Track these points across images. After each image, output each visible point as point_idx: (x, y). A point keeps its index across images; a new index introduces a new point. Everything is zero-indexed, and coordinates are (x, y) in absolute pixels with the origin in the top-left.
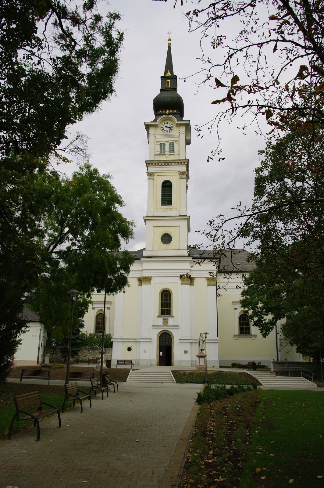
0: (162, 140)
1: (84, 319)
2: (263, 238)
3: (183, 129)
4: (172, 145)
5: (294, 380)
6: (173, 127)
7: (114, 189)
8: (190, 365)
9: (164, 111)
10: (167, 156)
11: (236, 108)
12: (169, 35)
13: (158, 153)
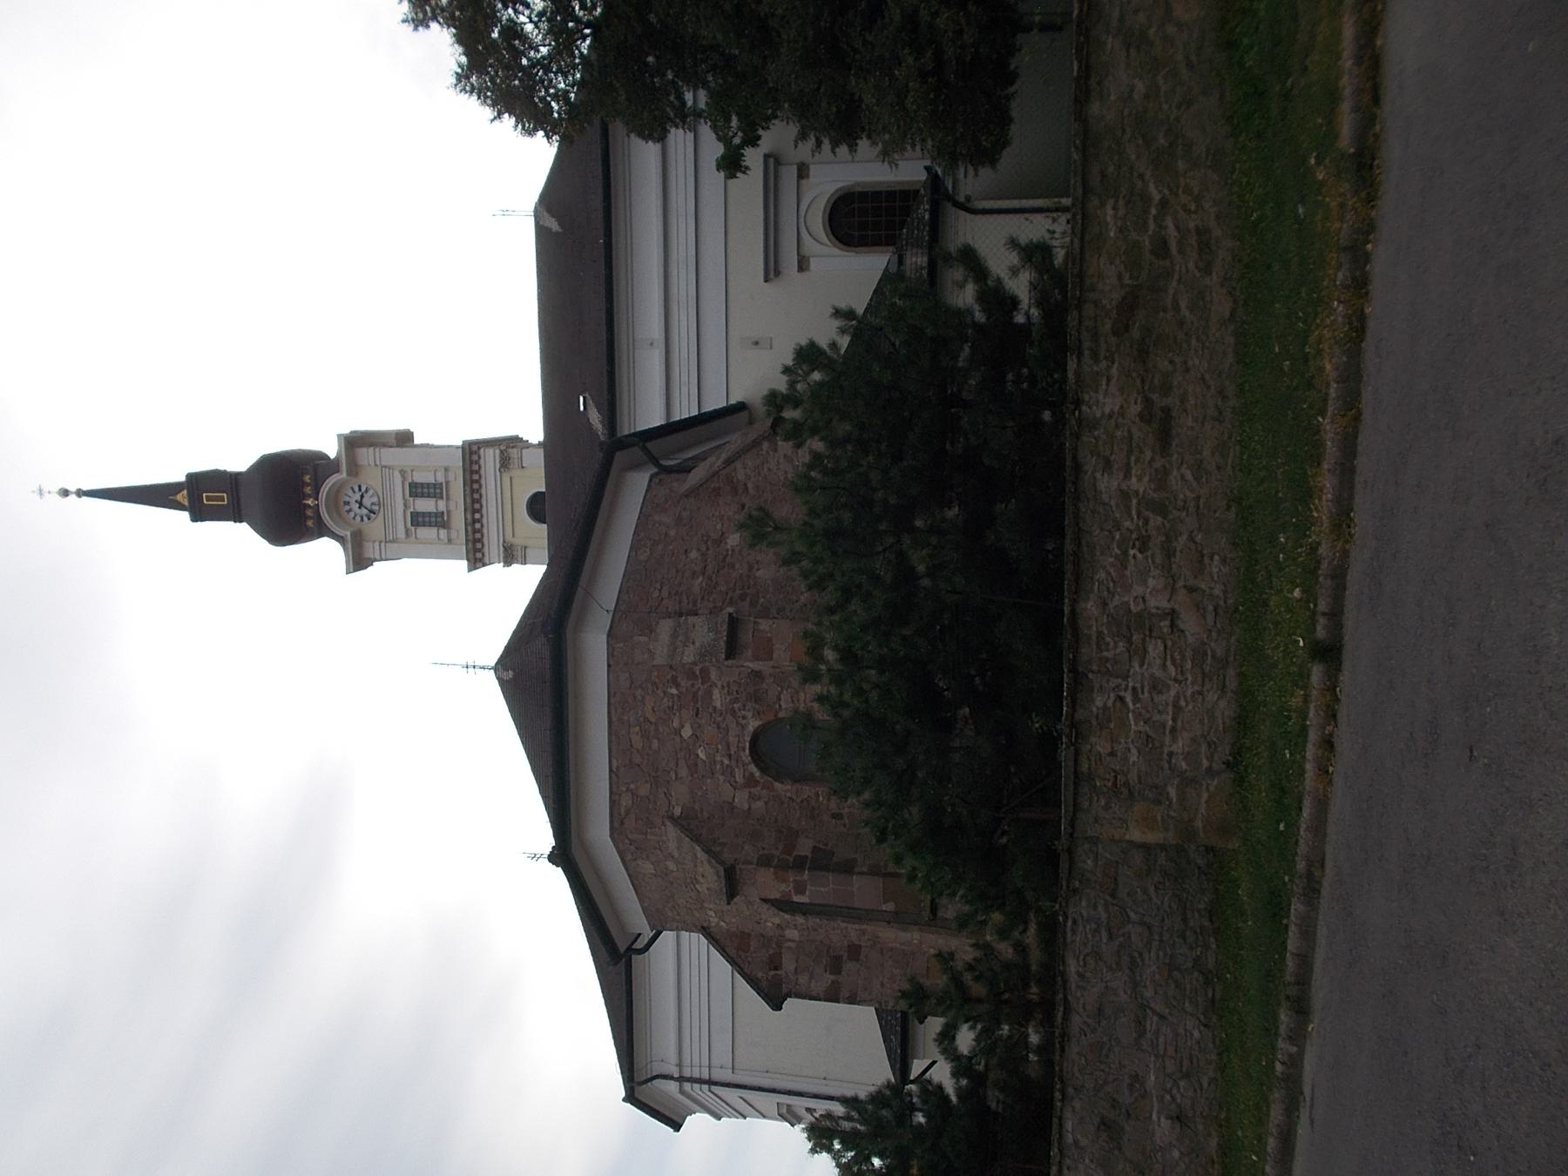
0: (400, 524)
1: (949, 1065)
3: (365, 455)
4: (417, 490)
6: (360, 487)
9: (309, 513)
12: (46, 495)
13: (443, 532)
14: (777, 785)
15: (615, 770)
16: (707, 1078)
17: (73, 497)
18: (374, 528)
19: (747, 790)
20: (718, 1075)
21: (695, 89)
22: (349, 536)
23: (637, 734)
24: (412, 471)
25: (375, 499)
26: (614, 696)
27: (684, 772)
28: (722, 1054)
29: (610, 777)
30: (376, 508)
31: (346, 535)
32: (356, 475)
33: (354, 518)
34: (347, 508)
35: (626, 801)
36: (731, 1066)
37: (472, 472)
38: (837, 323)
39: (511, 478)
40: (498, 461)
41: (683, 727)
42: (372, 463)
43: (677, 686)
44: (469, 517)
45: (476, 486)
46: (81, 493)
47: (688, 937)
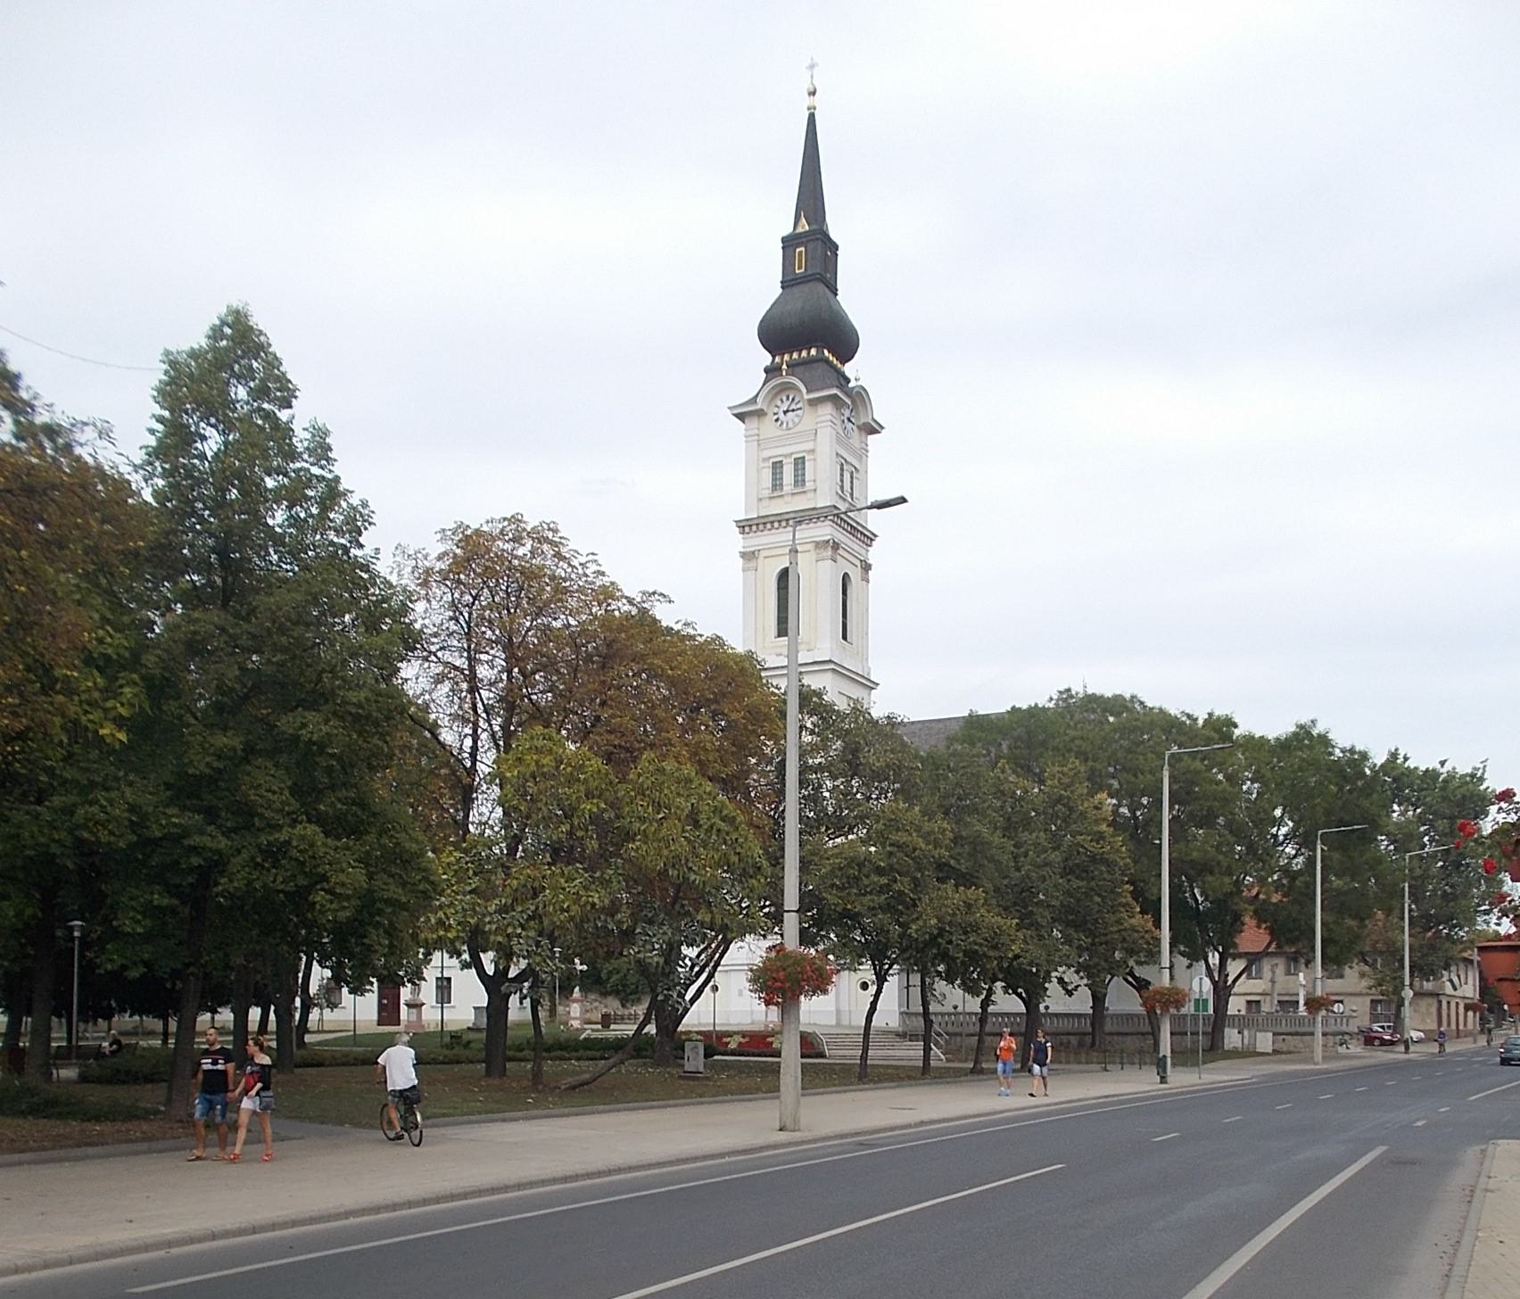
0: (775, 452)
2: (316, 954)
4: (800, 463)
8: (834, 1023)
10: (788, 499)
13: (767, 493)
17: (808, 101)
18: (768, 427)
21: (201, 1064)
38: (1206, 716)
46: (812, 119)
47: (1236, 997)
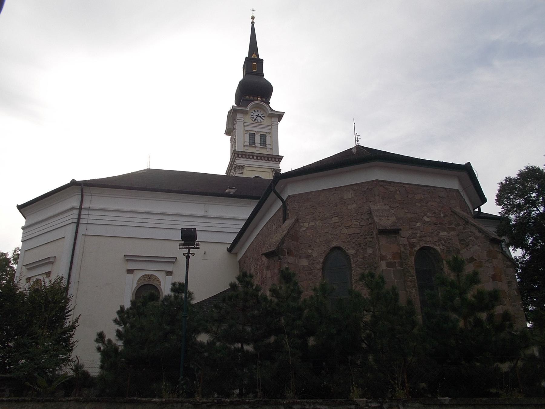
4: (263, 137)
5: (231, 226)
6: (264, 117)
7: (270, 338)
11: (189, 253)
12: (252, 12)
14: (413, 258)
15: (404, 186)
16: (80, 222)
19: (407, 243)
20: (82, 228)
22: (247, 109)
23: (421, 197)
24: (270, 136)
25: (259, 121)
26: (434, 189)
27: (409, 216)
28: (92, 230)
29: (401, 183)
30: (256, 121)
31: (248, 108)
32: (268, 116)
33: (255, 111)
34: (256, 111)
35: (392, 189)
36: (86, 234)
37: (272, 158)
39: (269, 172)
40: (276, 168)
41: (428, 217)
42: (273, 123)
43: (444, 217)
44: (255, 154)
45: (266, 159)
46: (253, 23)
